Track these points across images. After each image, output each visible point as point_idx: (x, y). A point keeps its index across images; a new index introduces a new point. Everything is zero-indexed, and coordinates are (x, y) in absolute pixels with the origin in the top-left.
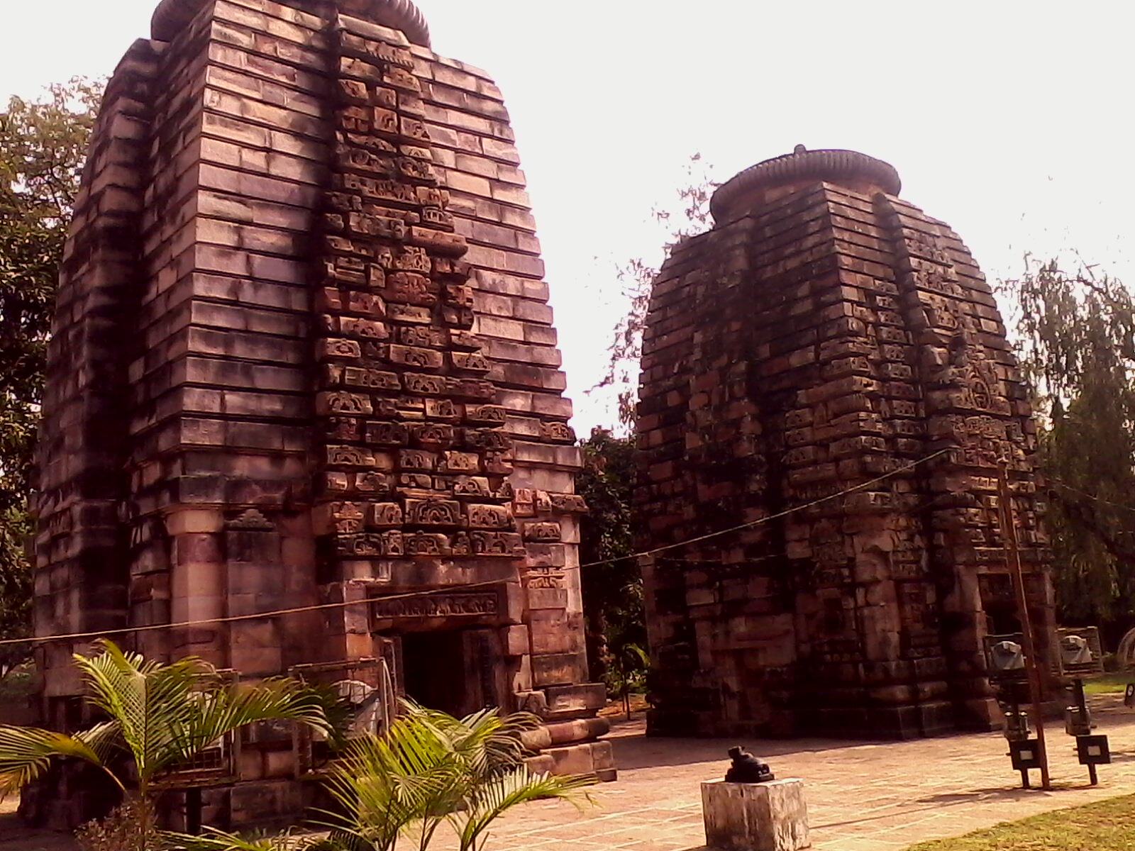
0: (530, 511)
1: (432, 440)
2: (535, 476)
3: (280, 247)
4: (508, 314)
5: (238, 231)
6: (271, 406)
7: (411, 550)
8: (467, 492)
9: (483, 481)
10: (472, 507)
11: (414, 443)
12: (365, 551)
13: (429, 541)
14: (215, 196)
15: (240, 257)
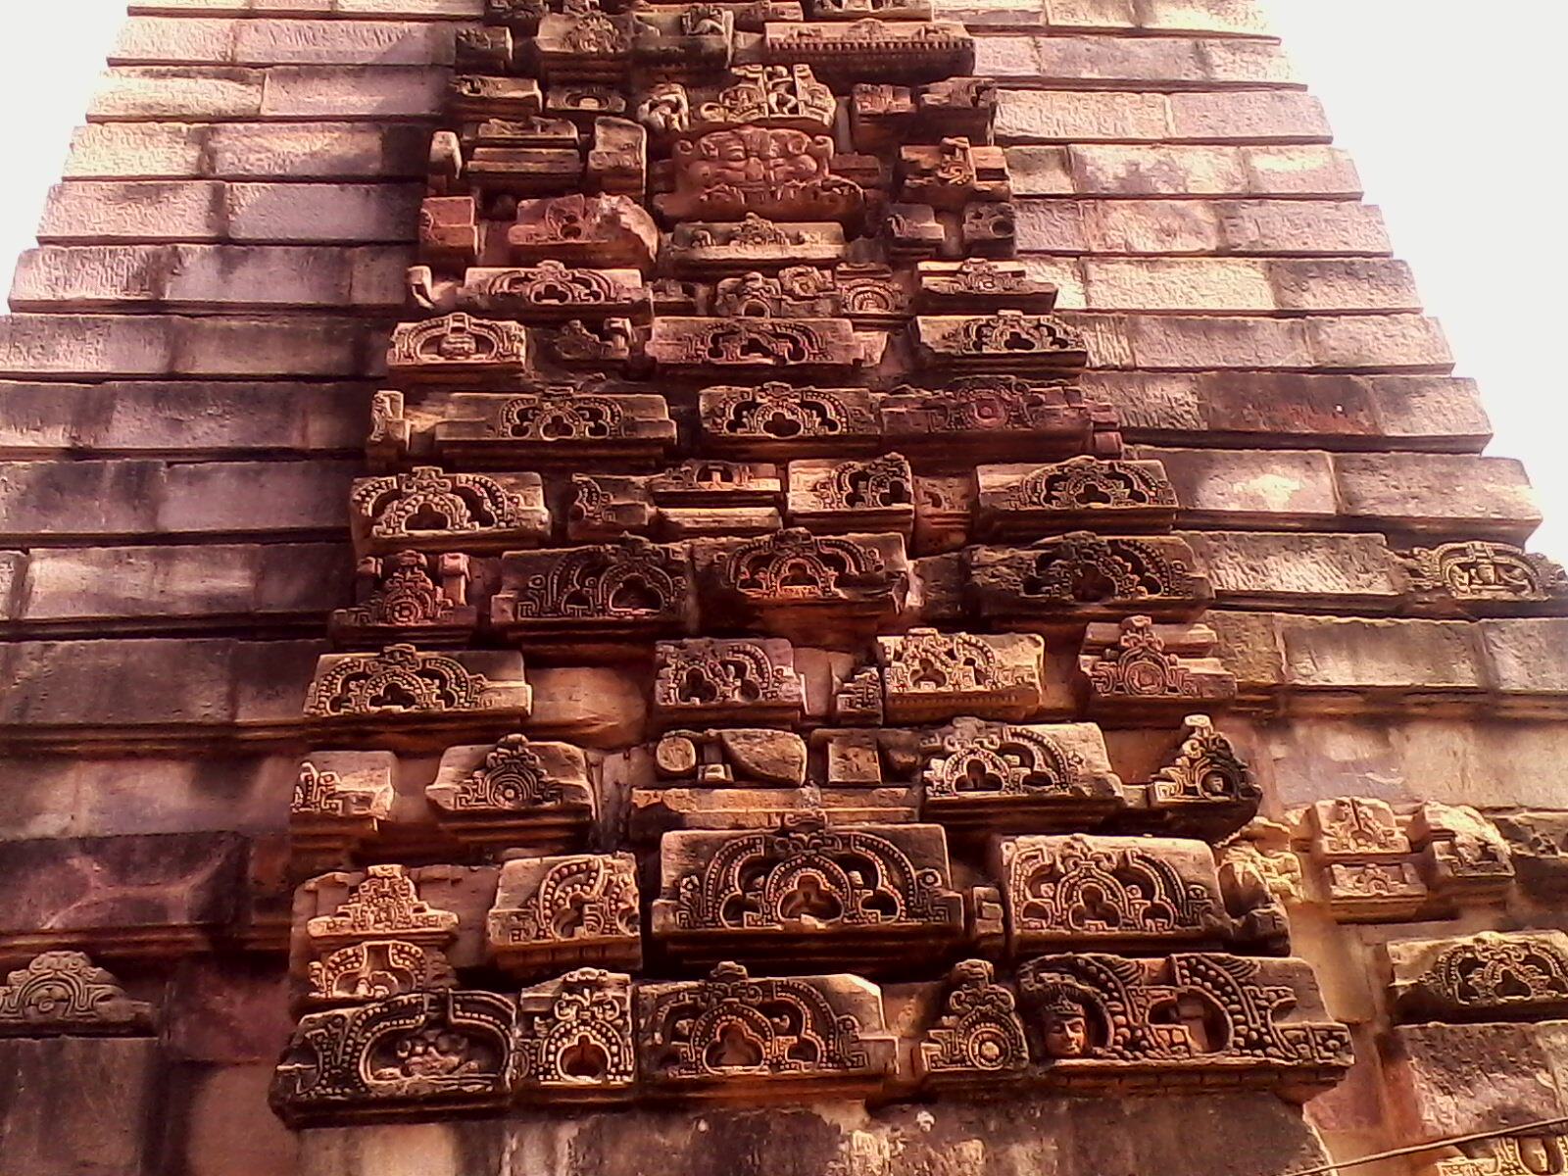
0: (1407, 887)
1: (800, 591)
2: (1411, 751)
3: (339, 158)
4: (1196, 245)
5: (201, 140)
6: (191, 582)
7: (672, 1058)
8: (994, 783)
9: (1084, 745)
10: (1013, 850)
11: (730, 615)
12: (430, 1069)
14: (144, 74)
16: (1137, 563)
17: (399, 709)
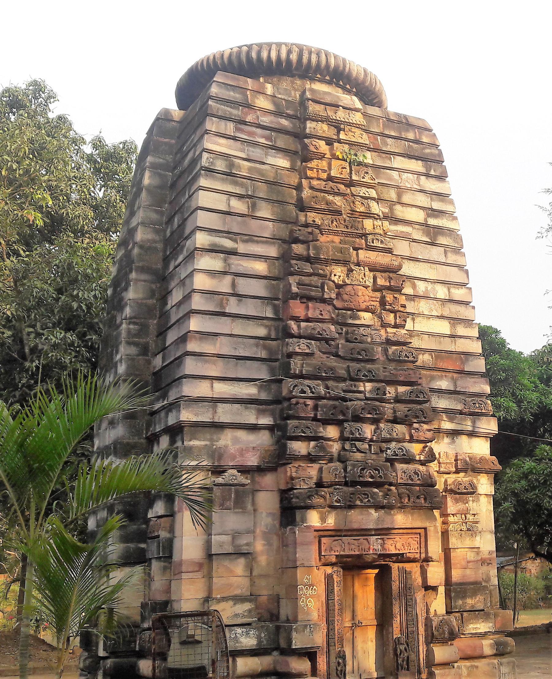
1: (369, 416)
8: (397, 455)
13: (365, 494)
15: (228, 279)
16: (423, 412)
17: (303, 434)
